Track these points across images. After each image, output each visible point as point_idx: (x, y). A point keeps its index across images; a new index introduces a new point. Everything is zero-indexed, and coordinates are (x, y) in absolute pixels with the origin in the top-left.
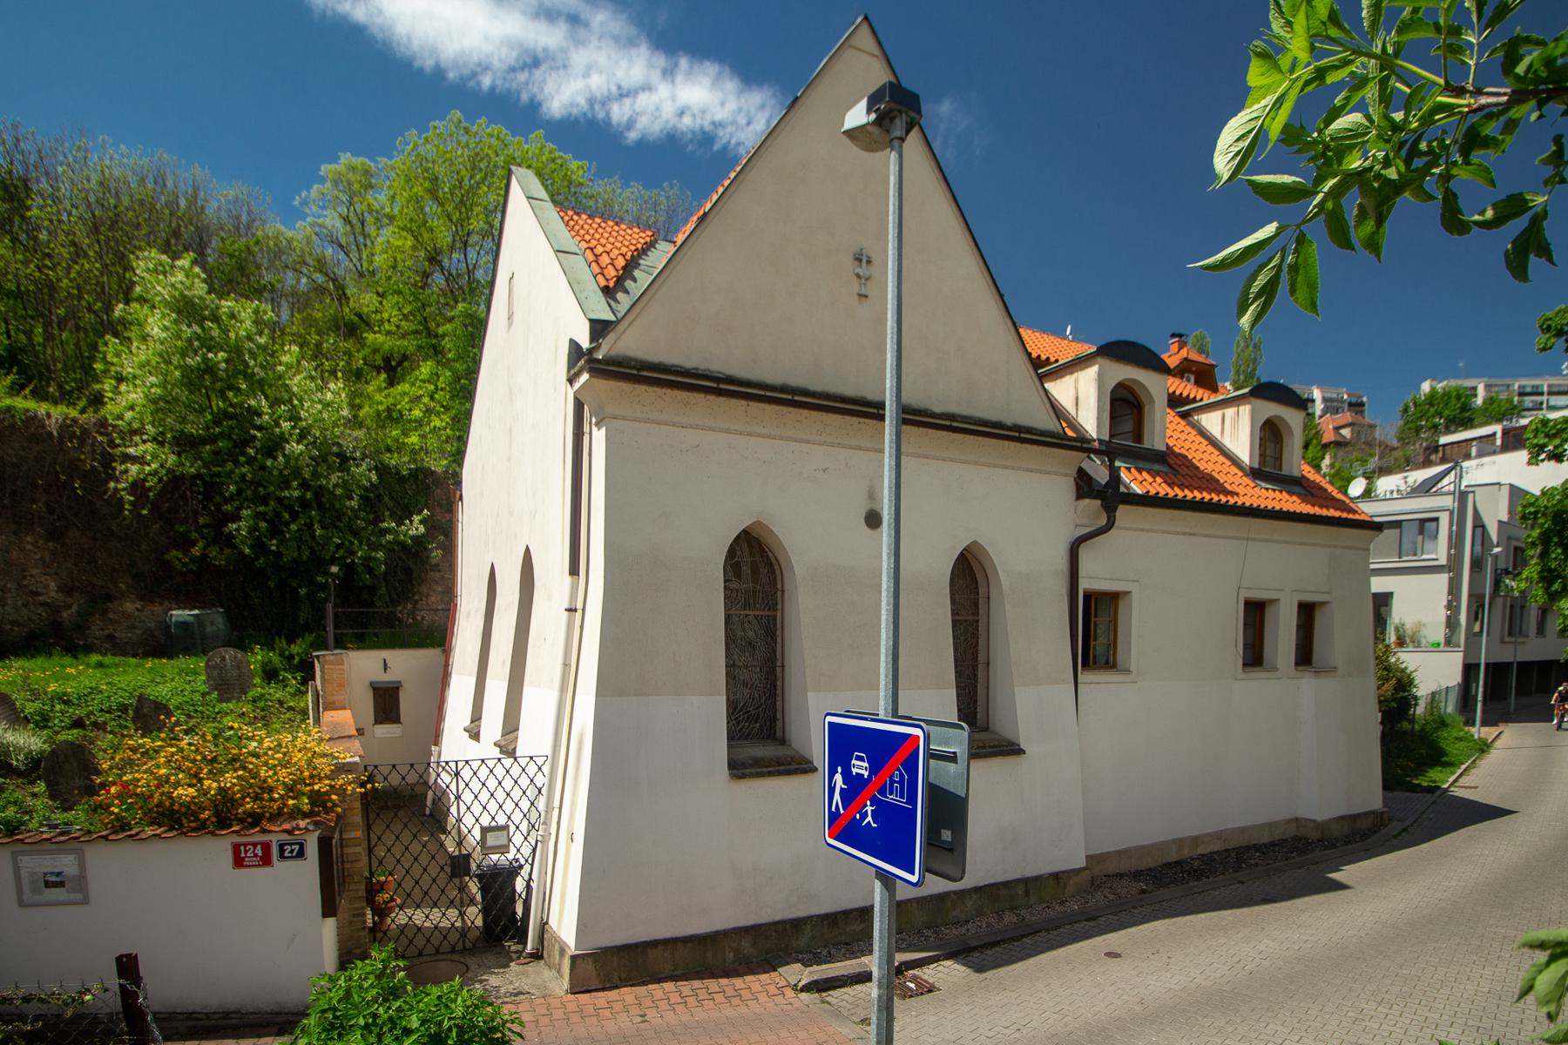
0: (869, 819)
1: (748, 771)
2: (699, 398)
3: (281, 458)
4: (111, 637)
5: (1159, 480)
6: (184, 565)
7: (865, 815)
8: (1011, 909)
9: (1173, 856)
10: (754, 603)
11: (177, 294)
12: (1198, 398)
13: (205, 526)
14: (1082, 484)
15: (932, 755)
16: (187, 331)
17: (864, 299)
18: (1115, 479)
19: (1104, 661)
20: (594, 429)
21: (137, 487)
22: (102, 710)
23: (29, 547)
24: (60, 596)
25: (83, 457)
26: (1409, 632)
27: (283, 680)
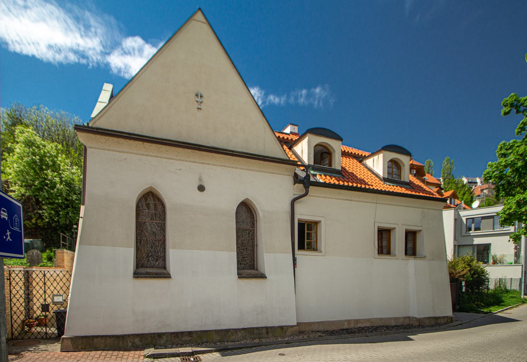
0: (9, 238)
6: (30, 225)
7: (7, 237)
10: (156, 217)
14: (295, 178)
17: (199, 110)
18: (308, 176)
26: (498, 259)
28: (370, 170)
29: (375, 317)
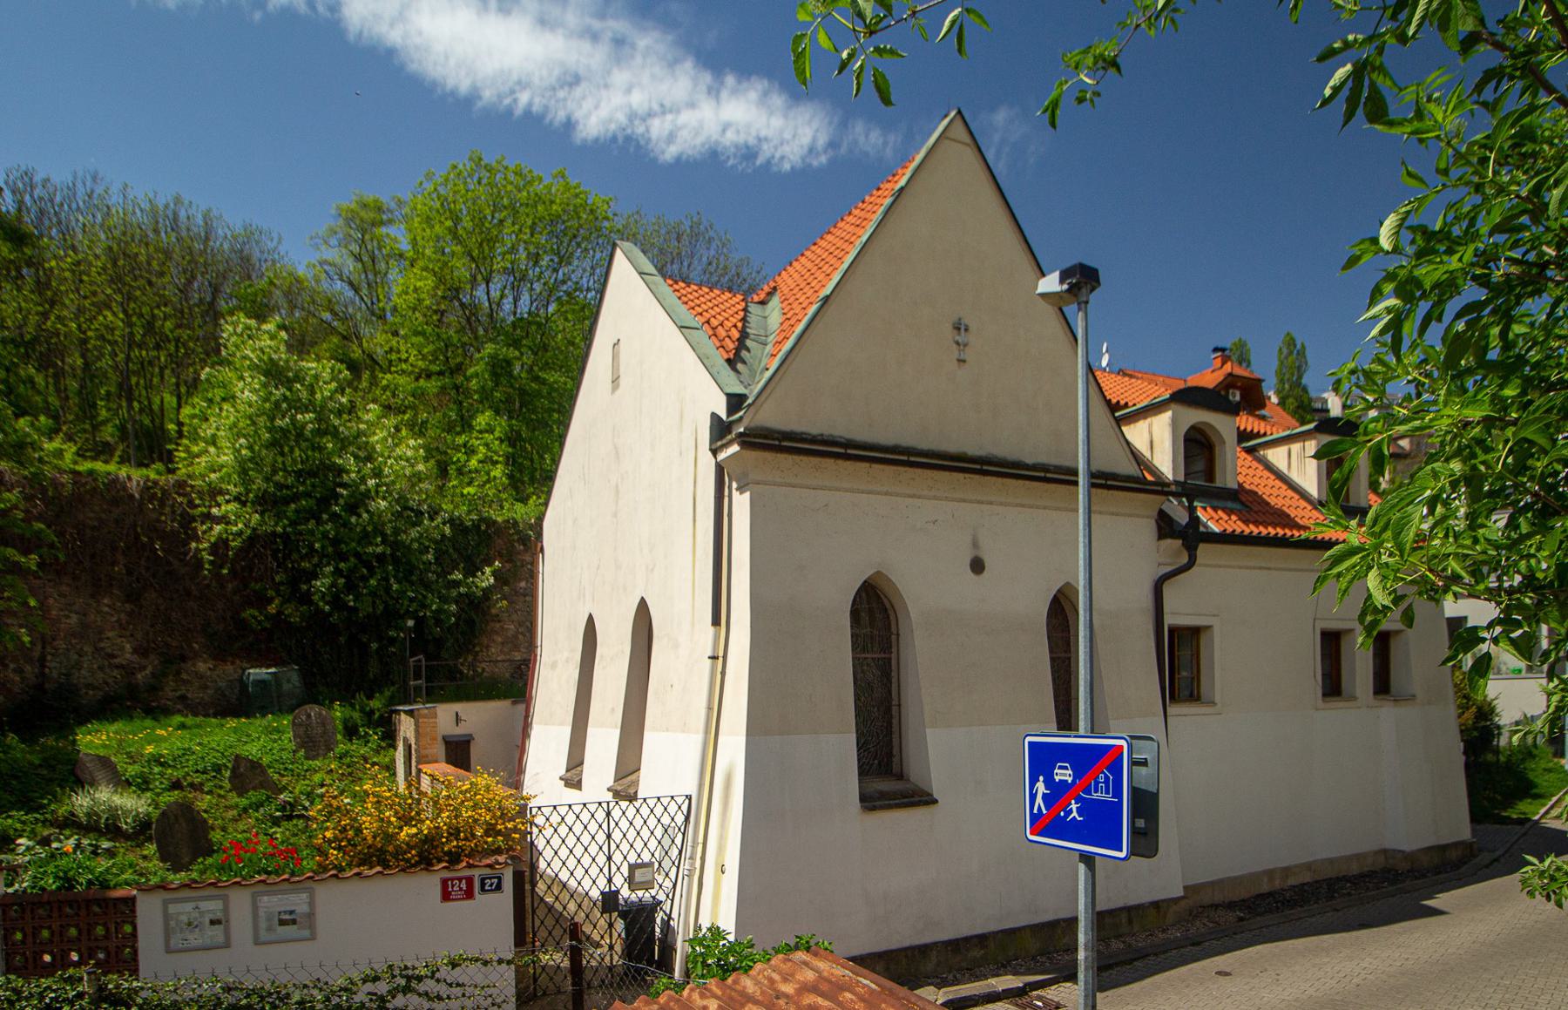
1: (878, 803)
2: (829, 462)
3: (365, 515)
4: (183, 698)
5: (1234, 518)
6: (259, 622)
8: (1117, 937)
9: (1265, 888)
11: (265, 358)
12: (1262, 432)
13: (281, 583)
15: (1134, 763)
16: (277, 394)
18: (1195, 520)
19: (1187, 693)
20: (735, 494)
21: (219, 547)
22: (197, 771)
23: (106, 609)
24: (135, 658)
25: (163, 518)
27: (364, 737)
28: (1280, 476)
29: (1318, 857)
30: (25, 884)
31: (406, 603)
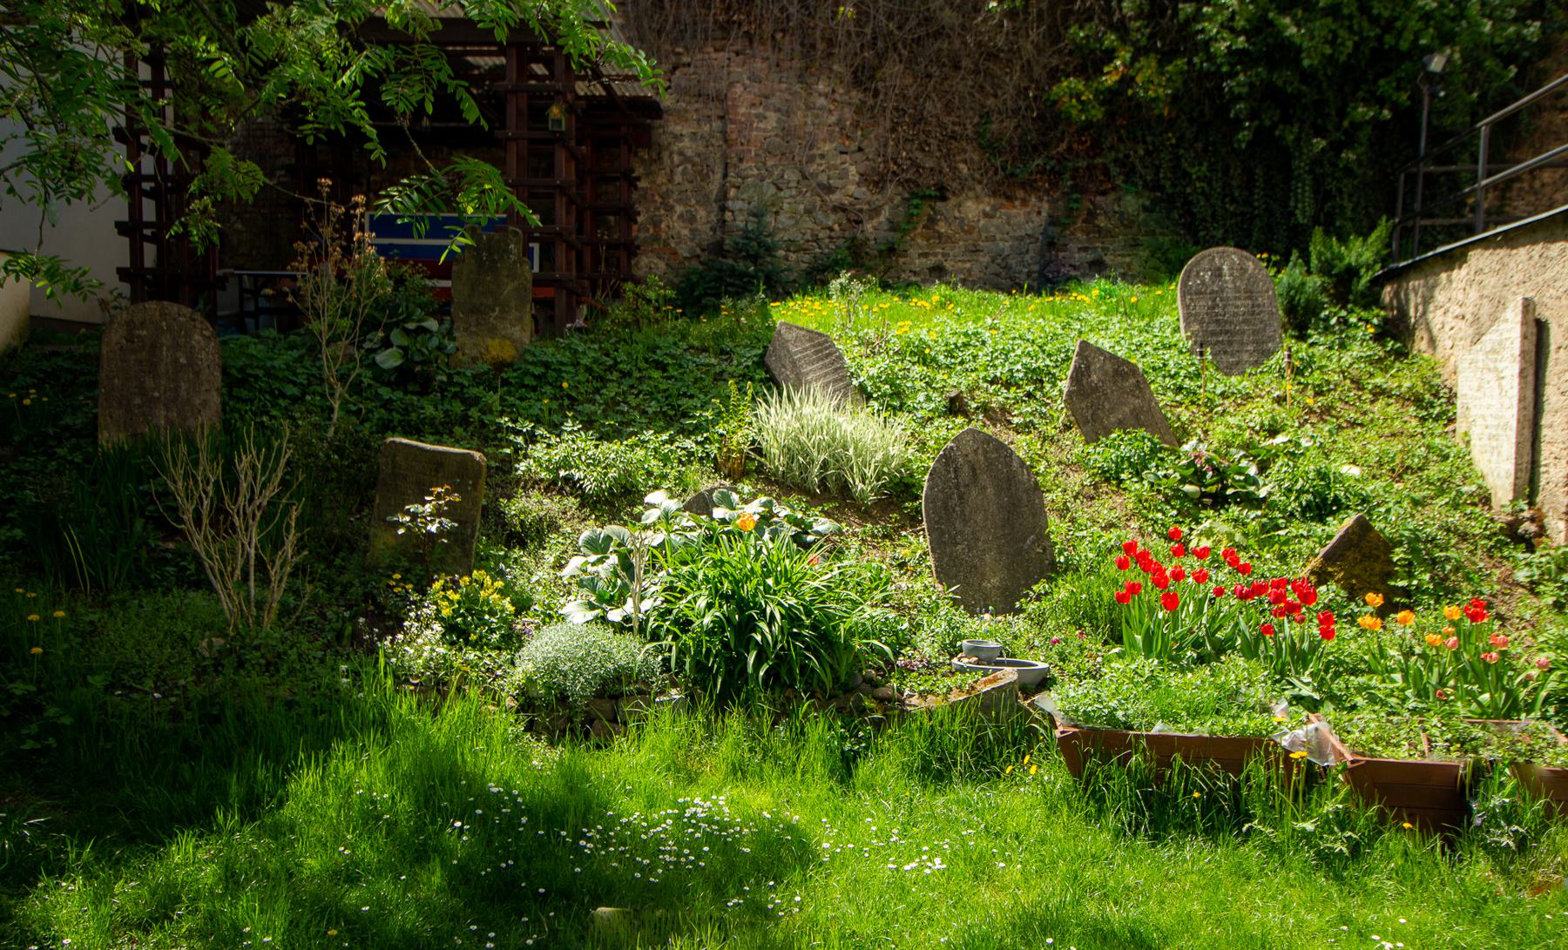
23: (822, 101)
24: (862, 192)
30: (646, 605)
31: (1414, 24)
